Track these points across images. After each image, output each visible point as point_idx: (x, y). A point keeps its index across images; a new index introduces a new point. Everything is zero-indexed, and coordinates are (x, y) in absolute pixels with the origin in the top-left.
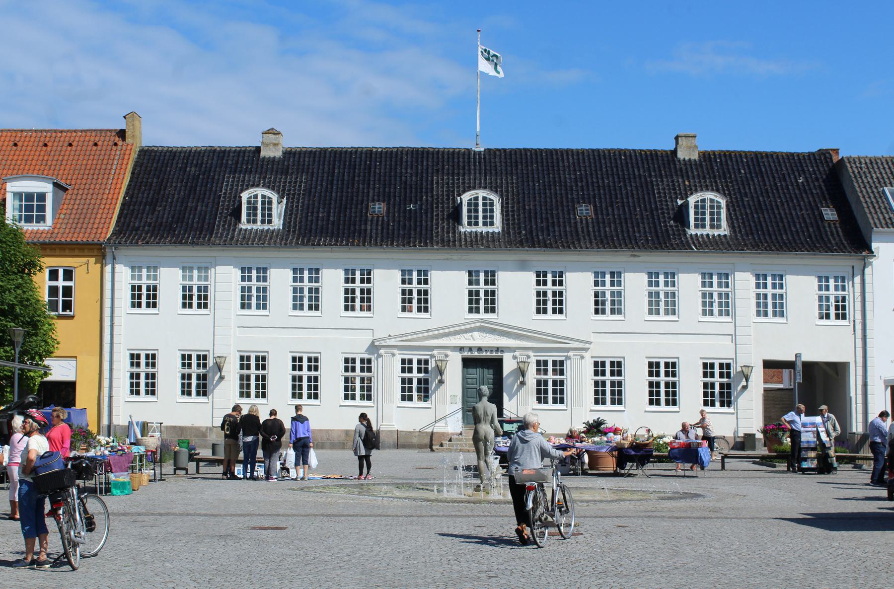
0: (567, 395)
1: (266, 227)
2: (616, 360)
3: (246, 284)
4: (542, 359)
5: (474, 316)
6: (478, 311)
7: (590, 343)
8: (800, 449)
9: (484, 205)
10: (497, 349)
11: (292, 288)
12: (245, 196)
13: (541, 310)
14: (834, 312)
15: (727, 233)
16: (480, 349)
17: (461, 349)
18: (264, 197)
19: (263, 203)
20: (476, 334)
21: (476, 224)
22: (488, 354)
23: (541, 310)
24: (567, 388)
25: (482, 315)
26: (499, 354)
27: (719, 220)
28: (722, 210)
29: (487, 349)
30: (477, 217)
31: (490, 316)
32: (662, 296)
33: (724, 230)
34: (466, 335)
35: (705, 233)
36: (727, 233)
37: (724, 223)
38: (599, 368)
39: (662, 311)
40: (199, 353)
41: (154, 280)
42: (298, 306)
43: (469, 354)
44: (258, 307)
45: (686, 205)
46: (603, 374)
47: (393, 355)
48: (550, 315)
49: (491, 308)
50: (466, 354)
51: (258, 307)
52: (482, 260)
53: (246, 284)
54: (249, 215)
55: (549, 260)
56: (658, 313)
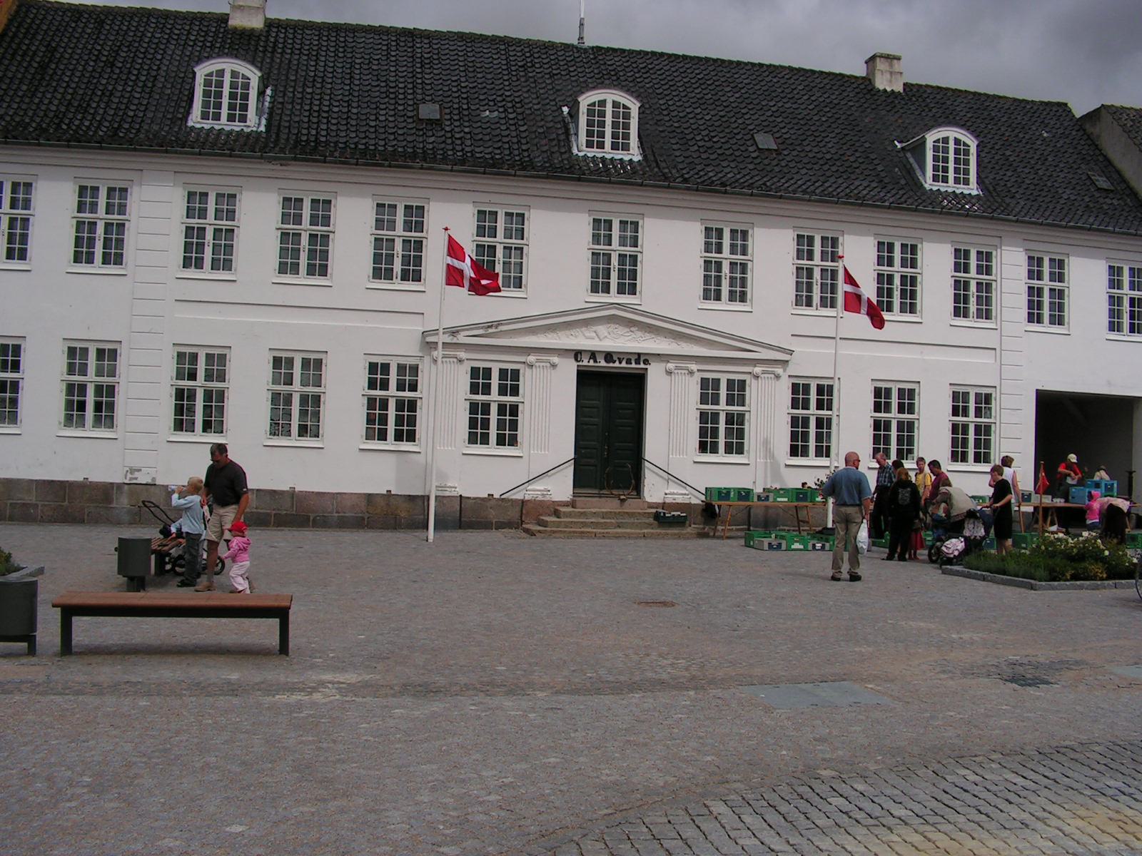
0: (523, 432)
1: (237, 126)
2: (313, 356)
3: (195, 222)
4: (482, 365)
5: (602, 298)
6: (607, 290)
7: (791, 352)
8: (745, 538)
9: (615, 115)
10: (639, 357)
11: (74, 221)
12: (202, 71)
13: (712, 293)
14: (102, 250)
15: (637, 157)
16: (609, 356)
17: (577, 354)
18: (234, 74)
19: (233, 85)
20: (602, 329)
21: (945, 180)
22: (624, 364)
23: (712, 293)
24: (422, 415)
25: (614, 297)
26: (642, 366)
27: (626, 136)
28: (971, 157)
29: (622, 356)
30: (602, 135)
31: (626, 299)
32: (726, 268)
33: (634, 154)
34: (589, 332)
35: (627, 158)
36: (637, 157)
37: (634, 141)
38: (799, 393)
39: (614, 287)
40: (101, 346)
41: (119, 214)
42: (804, 299)
43: (592, 363)
44: (106, 261)
45: (922, 143)
46: (385, 385)
47: (778, 377)
48: (724, 304)
49: (629, 285)
50: (585, 363)
51: (106, 261)
52: (617, 209)
53: (195, 222)
54: (206, 105)
55: (728, 216)
56: (718, 298)
